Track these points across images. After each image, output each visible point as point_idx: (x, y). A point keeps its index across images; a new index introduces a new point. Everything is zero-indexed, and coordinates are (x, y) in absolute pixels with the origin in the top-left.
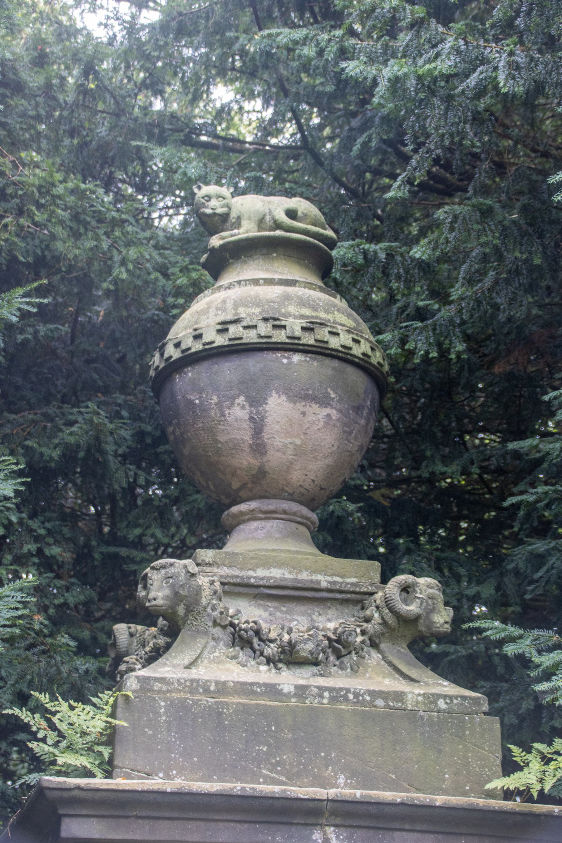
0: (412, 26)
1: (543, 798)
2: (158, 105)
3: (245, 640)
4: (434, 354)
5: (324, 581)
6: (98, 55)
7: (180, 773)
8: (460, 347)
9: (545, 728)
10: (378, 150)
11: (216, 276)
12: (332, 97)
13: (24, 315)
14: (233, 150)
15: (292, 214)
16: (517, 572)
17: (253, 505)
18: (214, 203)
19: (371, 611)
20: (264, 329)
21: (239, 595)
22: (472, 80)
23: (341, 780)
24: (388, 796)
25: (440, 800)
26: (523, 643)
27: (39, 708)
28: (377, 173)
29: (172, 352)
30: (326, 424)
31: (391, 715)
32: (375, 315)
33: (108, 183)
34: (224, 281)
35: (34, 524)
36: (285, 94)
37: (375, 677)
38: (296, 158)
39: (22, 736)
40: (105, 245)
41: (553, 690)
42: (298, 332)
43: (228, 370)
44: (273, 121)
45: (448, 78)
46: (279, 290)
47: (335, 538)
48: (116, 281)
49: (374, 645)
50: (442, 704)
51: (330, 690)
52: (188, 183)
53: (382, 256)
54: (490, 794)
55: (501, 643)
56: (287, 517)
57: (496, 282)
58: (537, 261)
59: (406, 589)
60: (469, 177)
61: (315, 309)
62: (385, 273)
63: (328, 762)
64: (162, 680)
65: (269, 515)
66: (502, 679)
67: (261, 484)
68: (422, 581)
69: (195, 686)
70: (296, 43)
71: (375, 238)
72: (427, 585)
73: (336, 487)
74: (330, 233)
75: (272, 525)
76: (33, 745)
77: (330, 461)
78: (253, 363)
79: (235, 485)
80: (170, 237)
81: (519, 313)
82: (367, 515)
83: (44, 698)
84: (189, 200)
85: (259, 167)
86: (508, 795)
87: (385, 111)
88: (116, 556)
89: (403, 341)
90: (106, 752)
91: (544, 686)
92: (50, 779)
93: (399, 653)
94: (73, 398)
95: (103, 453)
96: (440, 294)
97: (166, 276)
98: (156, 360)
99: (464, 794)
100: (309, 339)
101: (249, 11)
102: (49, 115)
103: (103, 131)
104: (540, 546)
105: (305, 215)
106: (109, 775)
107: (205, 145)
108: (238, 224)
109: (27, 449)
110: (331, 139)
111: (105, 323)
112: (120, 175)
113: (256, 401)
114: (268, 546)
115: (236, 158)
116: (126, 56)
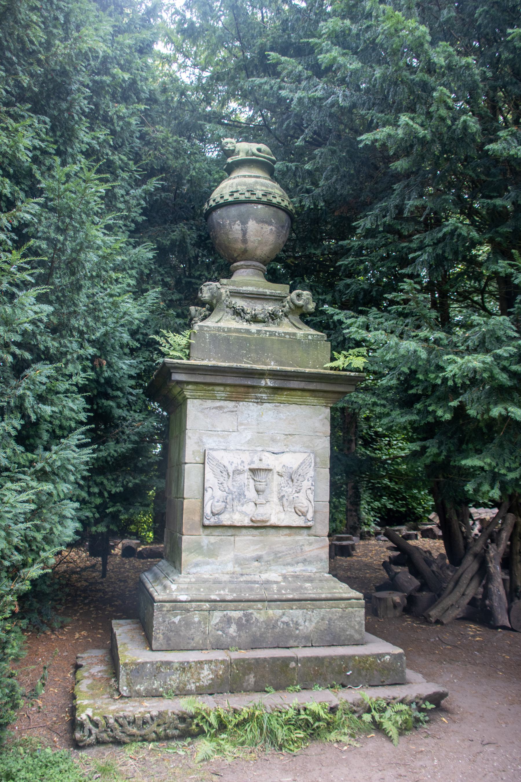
0: (307, 78)
1: (344, 370)
2: (209, 109)
3: (238, 313)
4: (312, 207)
5: (268, 292)
6: (186, 89)
7: (214, 360)
8: (322, 204)
9: (347, 347)
10: (293, 128)
11: (229, 174)
12: (276, 106)
13: (157, 189)
14: (237, 126)
15: (259, 150)
16: (340, 291)
17: (242, 263)
18: (229, 145)
19: (285, 303)
20: (248, 195)
21: (236, 296)
22: (329, 101)
23: (272, 363)
24: (289, 369)
25: (307, 370)
26: (340, 315)
27: (164, 336)
28: (293, 137)
29: (212, 203)
31: (291, 341)
32: (290, 192)
33: (189, 138)
34: (232, 176)
35: (160, 269)
36: (257, 104)
37: (285, 327)
38: (261, 130)
39: (157, 346)
40: (187, 162)
41: (349, 333)
42: (260, 196)
43: (233, 211)
44: (253, 116)
45: (320, 99)
46: (253, 180)
47: (273, 276)
48: (191, 176)
49: (286, 316)
50: (310, 337)
52: (219, 138)
53: (294, 168)
54: (325, 369)
55: (332, 315)
56: (255, 267)
57: (337, 180)
58: (352, 172)
59: (299, 295)
60: (326, 139)
61: (267, 187)
62: (295, 175)
64: (207, 327)
65: (248, 267)
66: (332, 329)
67: (245, 255)
68: (305, 292)
69: (219, 329)
70: (262, 84)
71: (291, 161)
72: (306, 294)
73: (274, 257)
74: (274, 158)
76: (161, 348)
77: (271, 247)
78: (243, 208)
79: (235, 255)
80: (212, 160)
81: (345, 192)
82: (287, 266)
83: (165, 332)
84: (220, 145)
85: (245, 132)
86: (331, 368)
87: (296, 111)
88: (190, 282)
89: (301, 201)
90: (187, 351)
91: (347, 331)
92: (167, 360)
93: (295, 319)
94: (175, 221)
95: (186, 243)
96: (315, 184)
97: (210, 174)
98: (206, 206)
100: (265, 199)
101: (244, 72)
102: (167, 112)
103: (187, 118)
104: (349, 281)
106: (188, 359)
107: (227, 125)
108: (238, 154)
109: (157, 241)
110: (275, 123)
111: (187, 193)
112: (193, 135)
113: (244, 223)
114: (247, 278)
115: (238, 130)
116: (196, 89)
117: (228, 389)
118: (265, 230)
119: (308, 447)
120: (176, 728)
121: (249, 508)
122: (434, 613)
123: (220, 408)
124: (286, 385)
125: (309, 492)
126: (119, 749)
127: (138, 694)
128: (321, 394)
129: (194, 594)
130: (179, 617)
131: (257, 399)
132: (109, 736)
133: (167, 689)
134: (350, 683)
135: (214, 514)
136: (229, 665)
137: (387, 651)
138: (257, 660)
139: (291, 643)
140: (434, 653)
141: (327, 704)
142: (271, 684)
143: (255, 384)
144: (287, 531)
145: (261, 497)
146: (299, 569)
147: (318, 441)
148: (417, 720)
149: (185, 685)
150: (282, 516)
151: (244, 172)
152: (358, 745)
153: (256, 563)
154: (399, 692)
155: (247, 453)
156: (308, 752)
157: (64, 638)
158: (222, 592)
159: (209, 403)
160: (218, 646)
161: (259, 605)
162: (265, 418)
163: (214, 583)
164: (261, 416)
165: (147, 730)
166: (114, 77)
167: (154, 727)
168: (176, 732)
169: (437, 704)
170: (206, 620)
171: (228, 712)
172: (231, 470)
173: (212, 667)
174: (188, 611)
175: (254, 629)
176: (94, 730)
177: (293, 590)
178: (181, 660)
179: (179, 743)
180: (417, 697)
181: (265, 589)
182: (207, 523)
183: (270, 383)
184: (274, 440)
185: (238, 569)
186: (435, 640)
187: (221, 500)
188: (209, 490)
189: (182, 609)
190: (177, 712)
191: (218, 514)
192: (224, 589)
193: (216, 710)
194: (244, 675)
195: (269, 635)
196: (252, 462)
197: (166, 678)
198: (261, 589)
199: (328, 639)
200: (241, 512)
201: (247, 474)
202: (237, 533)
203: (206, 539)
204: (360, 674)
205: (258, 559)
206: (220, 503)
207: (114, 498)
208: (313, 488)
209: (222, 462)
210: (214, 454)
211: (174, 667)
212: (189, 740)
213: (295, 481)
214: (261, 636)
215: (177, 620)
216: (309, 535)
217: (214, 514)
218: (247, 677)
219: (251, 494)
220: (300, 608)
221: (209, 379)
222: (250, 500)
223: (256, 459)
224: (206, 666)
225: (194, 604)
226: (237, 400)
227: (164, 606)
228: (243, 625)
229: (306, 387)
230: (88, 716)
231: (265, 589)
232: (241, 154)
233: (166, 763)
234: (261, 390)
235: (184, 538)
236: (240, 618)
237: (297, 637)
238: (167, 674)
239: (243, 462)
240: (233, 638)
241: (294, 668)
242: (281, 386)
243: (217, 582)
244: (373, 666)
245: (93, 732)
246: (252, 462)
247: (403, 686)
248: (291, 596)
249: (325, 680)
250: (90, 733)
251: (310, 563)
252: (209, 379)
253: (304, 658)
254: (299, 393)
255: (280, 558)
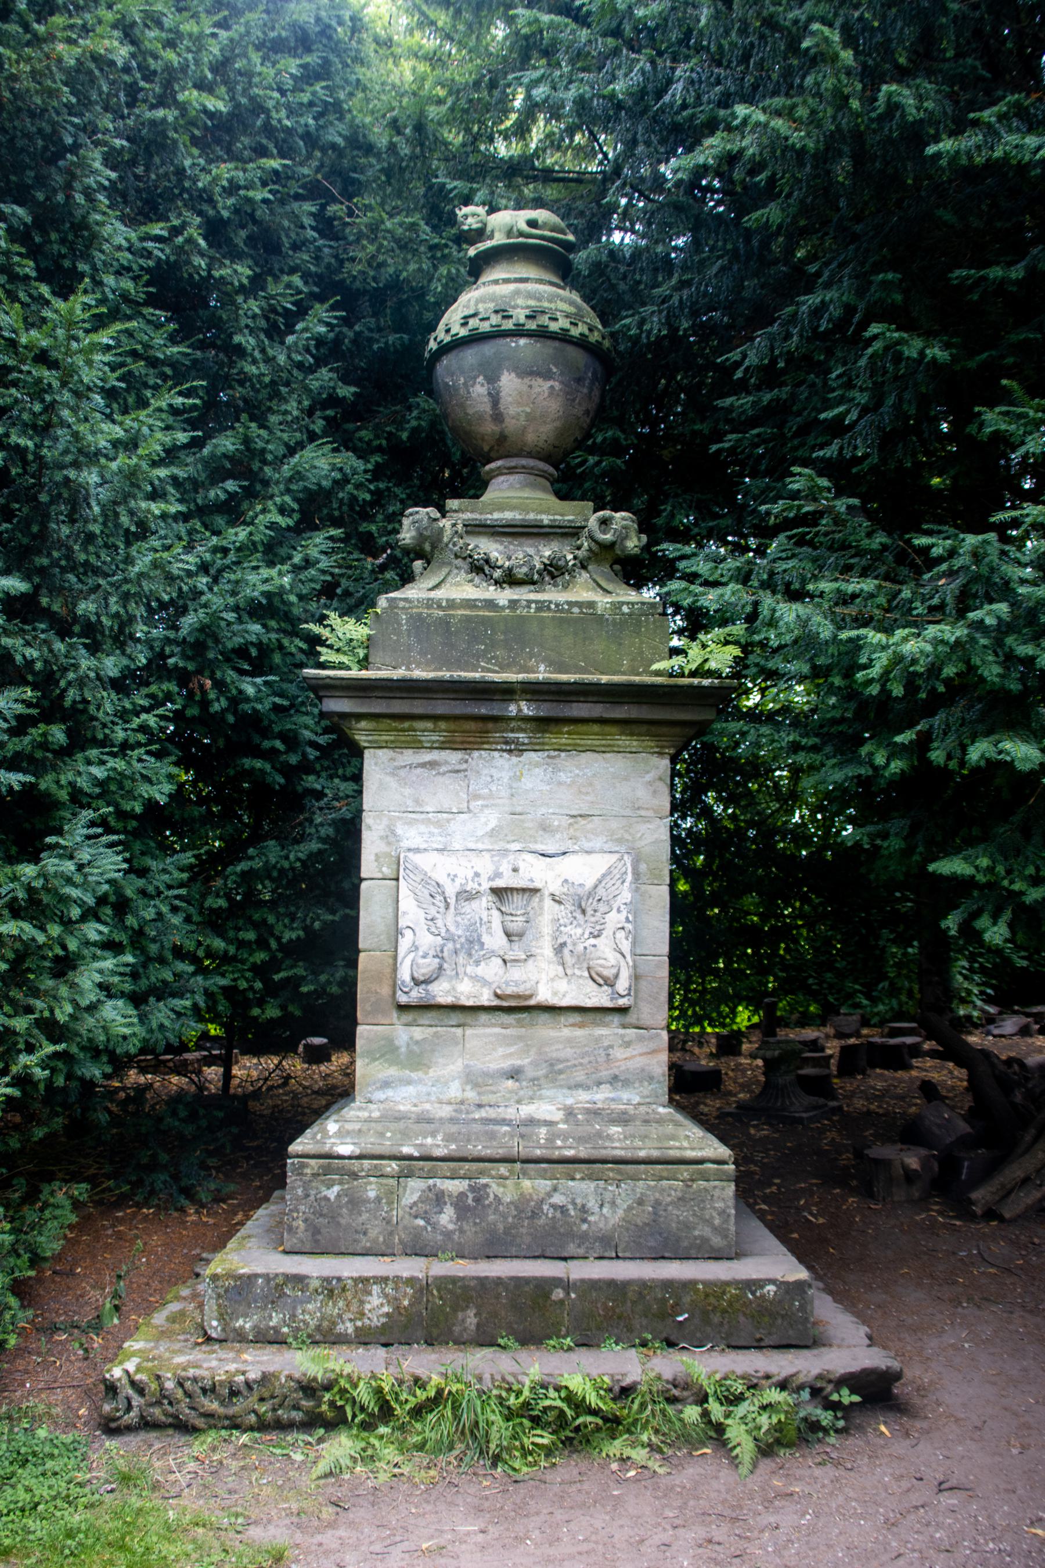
3: (480, 568)
5: (546, 519)
7: (418, 666)
15: (532, 223)
17: (499, 463)
18: (470, 220)
20: (495, 319)
21: (479, 534)
23: (542, 668)
30: (551, 394)
37: (585, 591)
42: (522, 320)
43: (470, 356)
46: (512, 287)
47: (567, 484)
49: (584, 567)
50: (625, 609)
51: (536, 602)
54: (658, 673)
61: (539, 300)
63: (531, 656)
64: (406, 600)
65: (511, 470)
67: (504, 447)
68: (618, 515)
69: (429, 603)
74: (571, 237)
75: (514, 479)
77: (558, 424)
78: (488, 349)
79: (486, 448)
93: (601, 571)
99: (638, 674)
100: (532, 325)
105: (545, 223)
108: (491, 237)
113: (492, 379)
117: (443, 725)
118: (537, 390)
119: (620, 841)
120: (296, 1407)
121: (492, 970)
122: (981, 1195)
123: (432, 765)
124: (567, 713)
125: (621, 935)
126: (184, 1439)
127: (241, 1337)
128: (644, 728)
129: (370, 1143)
130: (336, 1189)
131: (506, 743)
132: (166, 1414)
133: (298, 1329)
134: (685, 1339)
135: (417, 983)
136: (422, 1288)
137: (771, 1276)
138: (482, 1281)
139: (572, 1249)
140: (955, 1283)
141: (606, 1379)
142: (511, 1332)
143: (495, 713)
144: (576, 1018)
145: (515, 946)
146: (601, 1096)
147: (643, 828)
148: (815, 1426)
149: (335, 1324)
150: (562, 985)
151: (497, 273)
152: (661, 1471)
153: (510, 1082)
154: (804, 1365)
155: (487, 855)
156: (549, 1476)
157: (211, 1221)
158: (429, 1141)
159: (409, 756)
160: (417, 1249)
161: (503, 1169)
162: (527, 783)
163: (419, 1121)
164: (517, 778)
165: (238, 1407)
166: (183, 108)
167: (252, 1402)
168: (297, 1416)
169: (877, 1393)
170: (392, 1196)
171: (401, 1382)
172: (451, 891)
173: (389, 1290)
174: (354, 1176)
175: (492, 1218)
176: (137, 1401)
177: (581, 1140)
178: (326, 1273)
179: (302, 1437)
180: (820, 1377)
181: (522, 1136)
182: (403, 999)
183: (527, 709)
184: (545, 828)
185: (471, 1095)
186: (970, 1255)
187: (432, 953)
188: (408, 933)
189: (341, 1171)
190: (297, 1375)
191: (427, 982)
192: (433, 1134)
193: (374, 1377)
194: (455, 1309)
195: (524, 1231)
196: (498, 875)
197: (295, 1308)
198: (512, 1137)
199: (652, 1243)
200: (475, 979)
201: (487, 900)
202: (469, 1020)
203: (406, 1034)
204: (706, 1321)
205: (514, 1074)
206: (427, 961)
207: (292, 951)
208: (629, 926)
209: (434, 876)
210: (416, 858)
211: (312, 1287)
212: (322, 1431)
213: (589, 912)
214: (507, 1231)
215: (332, 1193)
216: (624, 1027)
217: (417, 983)
218: (460, 1315)
219: (495, 940)
220: (590, 1177)
221: (398, 707)
222: (493, 954)
223: (505, 868)
224: (376, 1289)
225: (366, 1163)
226: (466, 746)
227: (306, 1166)
228: (468, 1208)
229: (606, 715)
230: (127, 1372)
231: (522, 1136)
232: (497, 235)
233: (255, 1475)
234: (513, 724)
235: (360, 1029)
236: (462, 1195)
237: (584, 1237)
238: (296, 1301)
239: (477, 875)
240: (448, 1234)
241: (561, 1302)
242: (552, 714)
243: (424, 1119)
244: (737, 1306)
245: (134, 1403)
246: (498, 875)
247: (805, 1352)
248: (570, 1153)
249: (630, 1330)
250: (129, 1408)
251: (627, 1083)
252: (398, 707)
253: (583, 1281)
254: (596, 728)
255: (561, 1072)
